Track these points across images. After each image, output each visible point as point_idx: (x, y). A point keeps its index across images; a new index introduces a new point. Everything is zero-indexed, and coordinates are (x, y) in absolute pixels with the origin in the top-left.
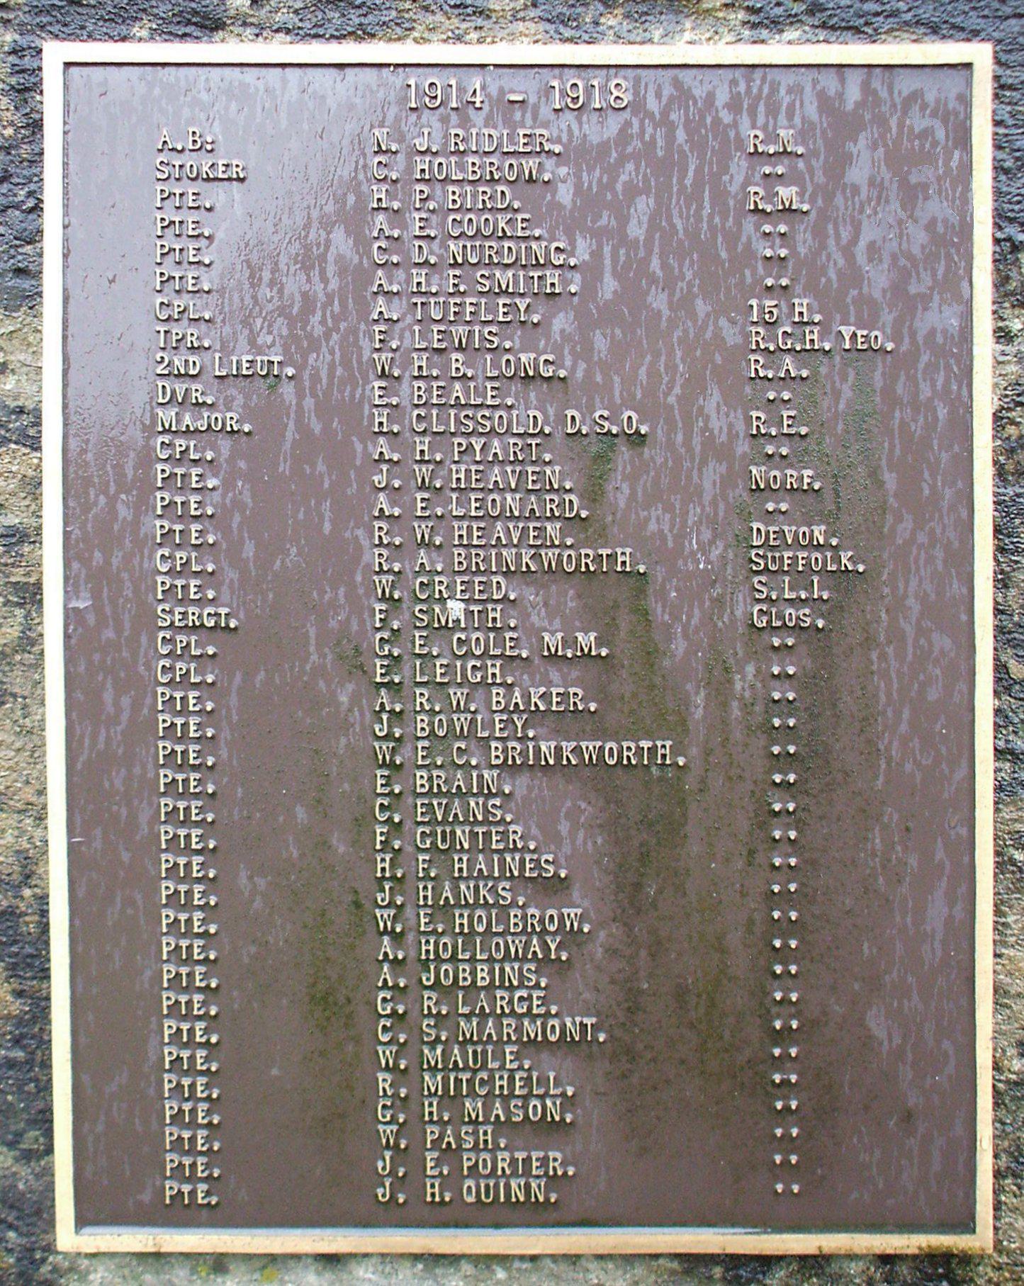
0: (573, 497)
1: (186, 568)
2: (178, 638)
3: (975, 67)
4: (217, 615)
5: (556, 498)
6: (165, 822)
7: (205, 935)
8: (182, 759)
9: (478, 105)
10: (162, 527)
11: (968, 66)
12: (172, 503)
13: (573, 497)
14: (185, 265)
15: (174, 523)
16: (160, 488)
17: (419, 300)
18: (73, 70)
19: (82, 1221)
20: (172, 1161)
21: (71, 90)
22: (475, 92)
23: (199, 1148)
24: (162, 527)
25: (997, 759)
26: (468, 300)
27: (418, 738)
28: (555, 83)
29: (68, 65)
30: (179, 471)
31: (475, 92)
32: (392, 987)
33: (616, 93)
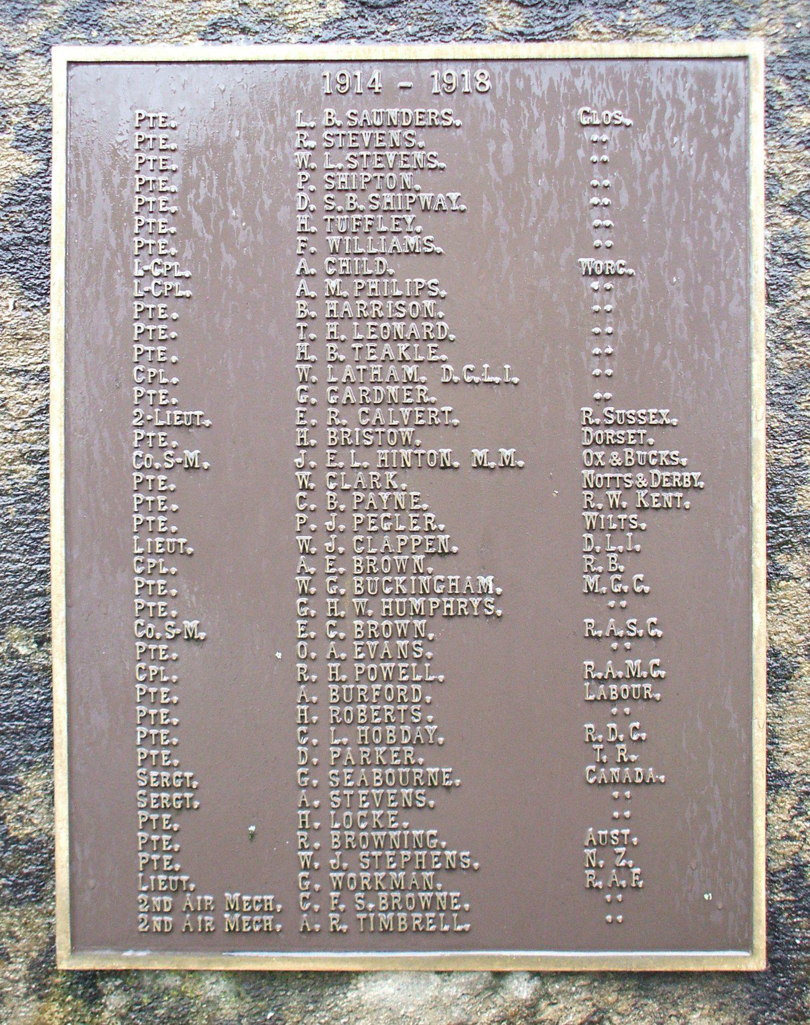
0: (444, 324)
1: (155, 571)
2: (151, 668)
3: (751, 61)
4: (183, 798)
5: (432, 326)
6: (141, 724)
7: (171, 851)
8: (155, 719)
9: (377, 90)
10: (138, 499)
11: (744, 58)
12: (150, 841)
13: (444, 324)
14: (156, 151)
15: (149, 708)
16: (137, 320)
17: (329, 217)
18: (76, 70)
19: (76, 946)
20: (141, 690)
21: (72, 382)
22: (374, 80)
23: (162, 743)
24: (139, 242)
25: (768, 702)
26: (367, 216)
27: (335, 850)
28: (435, 73)
29: (69, 63)
30: (152, 690)
31: (374, 80)
32: (308, 724)
33: (480, 80)
